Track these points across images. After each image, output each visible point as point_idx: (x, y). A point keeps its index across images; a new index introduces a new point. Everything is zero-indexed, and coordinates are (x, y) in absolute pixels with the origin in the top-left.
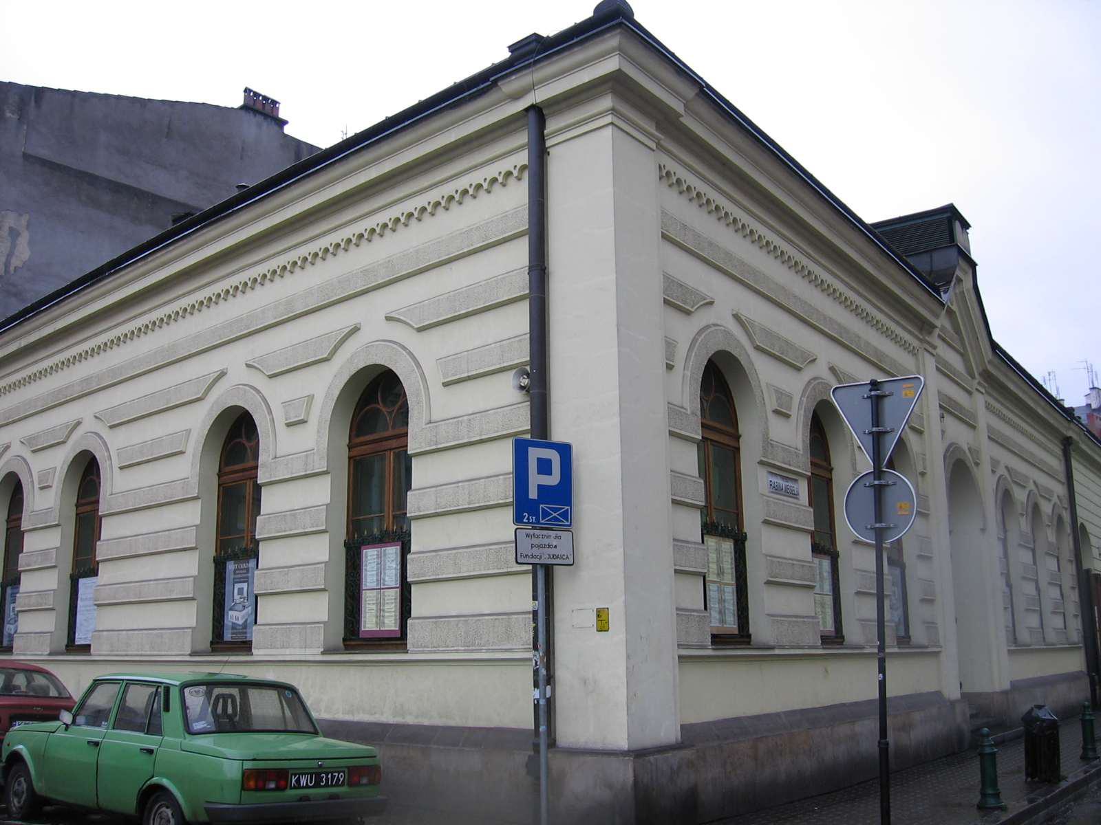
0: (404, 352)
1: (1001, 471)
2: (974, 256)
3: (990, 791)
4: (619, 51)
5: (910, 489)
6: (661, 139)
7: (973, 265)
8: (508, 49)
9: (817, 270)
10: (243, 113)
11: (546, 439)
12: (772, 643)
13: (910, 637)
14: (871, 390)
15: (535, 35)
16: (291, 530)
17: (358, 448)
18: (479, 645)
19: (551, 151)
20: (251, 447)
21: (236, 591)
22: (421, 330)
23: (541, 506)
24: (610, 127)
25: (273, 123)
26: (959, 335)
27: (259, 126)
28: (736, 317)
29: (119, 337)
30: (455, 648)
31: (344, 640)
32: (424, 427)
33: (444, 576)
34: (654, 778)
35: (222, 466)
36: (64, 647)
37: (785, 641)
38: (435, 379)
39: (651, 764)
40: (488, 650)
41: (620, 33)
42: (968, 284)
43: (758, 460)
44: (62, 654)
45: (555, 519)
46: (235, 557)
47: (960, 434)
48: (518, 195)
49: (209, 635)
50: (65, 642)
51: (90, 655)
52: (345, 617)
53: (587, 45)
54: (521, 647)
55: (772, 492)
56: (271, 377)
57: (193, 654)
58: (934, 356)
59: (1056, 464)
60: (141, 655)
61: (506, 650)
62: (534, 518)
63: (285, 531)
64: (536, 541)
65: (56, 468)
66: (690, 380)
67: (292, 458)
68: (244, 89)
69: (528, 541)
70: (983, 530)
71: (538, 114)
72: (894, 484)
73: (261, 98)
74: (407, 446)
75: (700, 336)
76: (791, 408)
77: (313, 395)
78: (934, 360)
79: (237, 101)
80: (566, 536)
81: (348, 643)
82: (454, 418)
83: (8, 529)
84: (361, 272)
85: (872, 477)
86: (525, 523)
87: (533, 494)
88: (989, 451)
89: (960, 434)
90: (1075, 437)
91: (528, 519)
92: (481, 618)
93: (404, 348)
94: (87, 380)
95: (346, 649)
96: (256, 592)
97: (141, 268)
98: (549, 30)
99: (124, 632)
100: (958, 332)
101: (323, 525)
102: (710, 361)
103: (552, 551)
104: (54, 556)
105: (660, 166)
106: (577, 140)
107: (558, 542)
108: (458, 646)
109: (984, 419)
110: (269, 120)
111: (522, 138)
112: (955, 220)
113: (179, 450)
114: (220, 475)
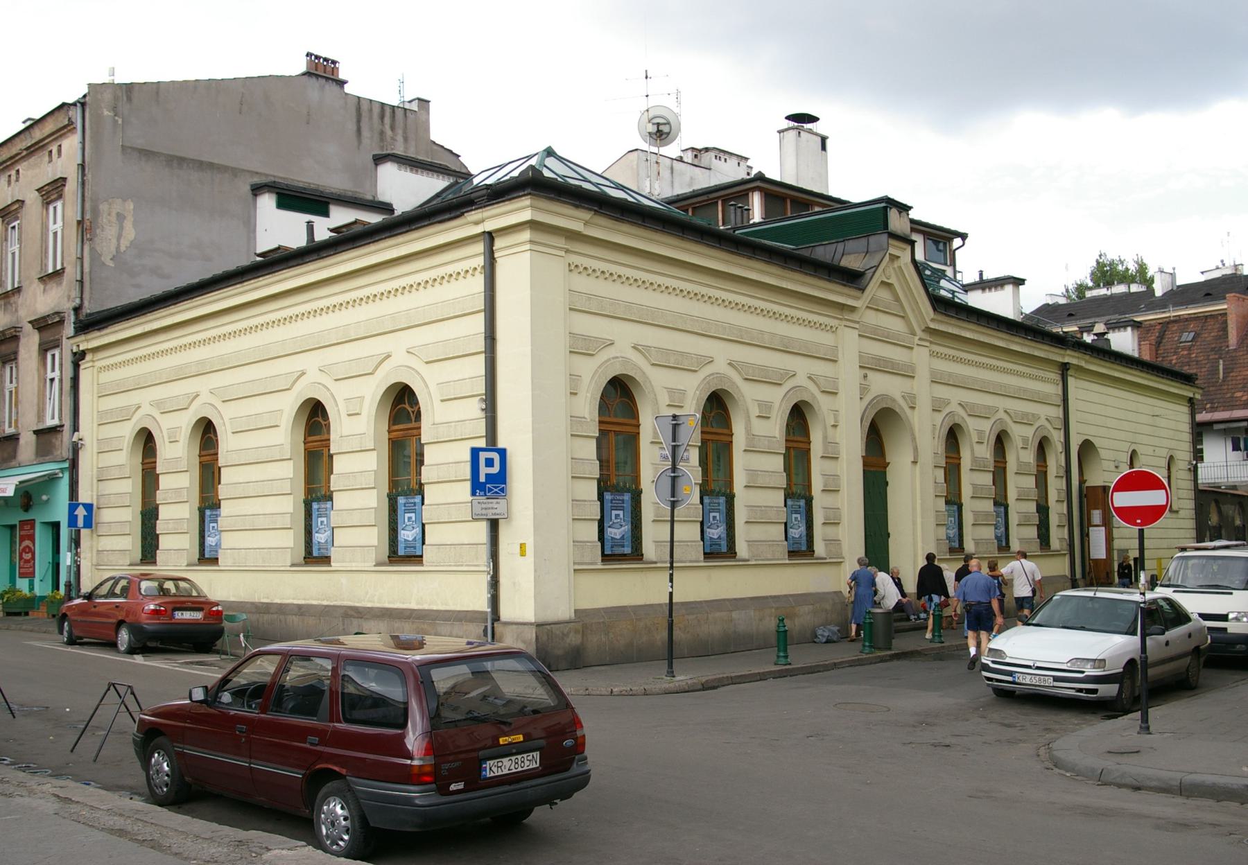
3: (782, 654)
10: (306, 78)
12: (655, 560)
18: (462, 562)
20: (325, 425)
21: (318, 522)
23: (488, 485)
25: (334, 83)
27: (322, 87)
31: (389, 557)
36: (197, 560)
38: (437, 398)
40: (467, 565)
41: (531, 198)
44: (196, 565)
45: (496, 492)
46: (318, 500)
47: (886, 386)
48: (478, 283)
49: (301, 552)
50: (197, 556)
57: (293, 565)
58: (857, 329)
64: (484, 506)
65: (181, 427)
71: (490, 237)
72: (683, 475)
73: (321, 60)
79: (301, 66)
80: (503, 502)
83: (143, 470)
85: (670, 471)
87: (482, 479)
93: (418, 373)
94: (200, 362)
96: (332, 525)
97: (238, 288)
99: (243, 550)
103: (494, 511)
104: (186, 494)
107: (496, 507)
111: (480, 247)
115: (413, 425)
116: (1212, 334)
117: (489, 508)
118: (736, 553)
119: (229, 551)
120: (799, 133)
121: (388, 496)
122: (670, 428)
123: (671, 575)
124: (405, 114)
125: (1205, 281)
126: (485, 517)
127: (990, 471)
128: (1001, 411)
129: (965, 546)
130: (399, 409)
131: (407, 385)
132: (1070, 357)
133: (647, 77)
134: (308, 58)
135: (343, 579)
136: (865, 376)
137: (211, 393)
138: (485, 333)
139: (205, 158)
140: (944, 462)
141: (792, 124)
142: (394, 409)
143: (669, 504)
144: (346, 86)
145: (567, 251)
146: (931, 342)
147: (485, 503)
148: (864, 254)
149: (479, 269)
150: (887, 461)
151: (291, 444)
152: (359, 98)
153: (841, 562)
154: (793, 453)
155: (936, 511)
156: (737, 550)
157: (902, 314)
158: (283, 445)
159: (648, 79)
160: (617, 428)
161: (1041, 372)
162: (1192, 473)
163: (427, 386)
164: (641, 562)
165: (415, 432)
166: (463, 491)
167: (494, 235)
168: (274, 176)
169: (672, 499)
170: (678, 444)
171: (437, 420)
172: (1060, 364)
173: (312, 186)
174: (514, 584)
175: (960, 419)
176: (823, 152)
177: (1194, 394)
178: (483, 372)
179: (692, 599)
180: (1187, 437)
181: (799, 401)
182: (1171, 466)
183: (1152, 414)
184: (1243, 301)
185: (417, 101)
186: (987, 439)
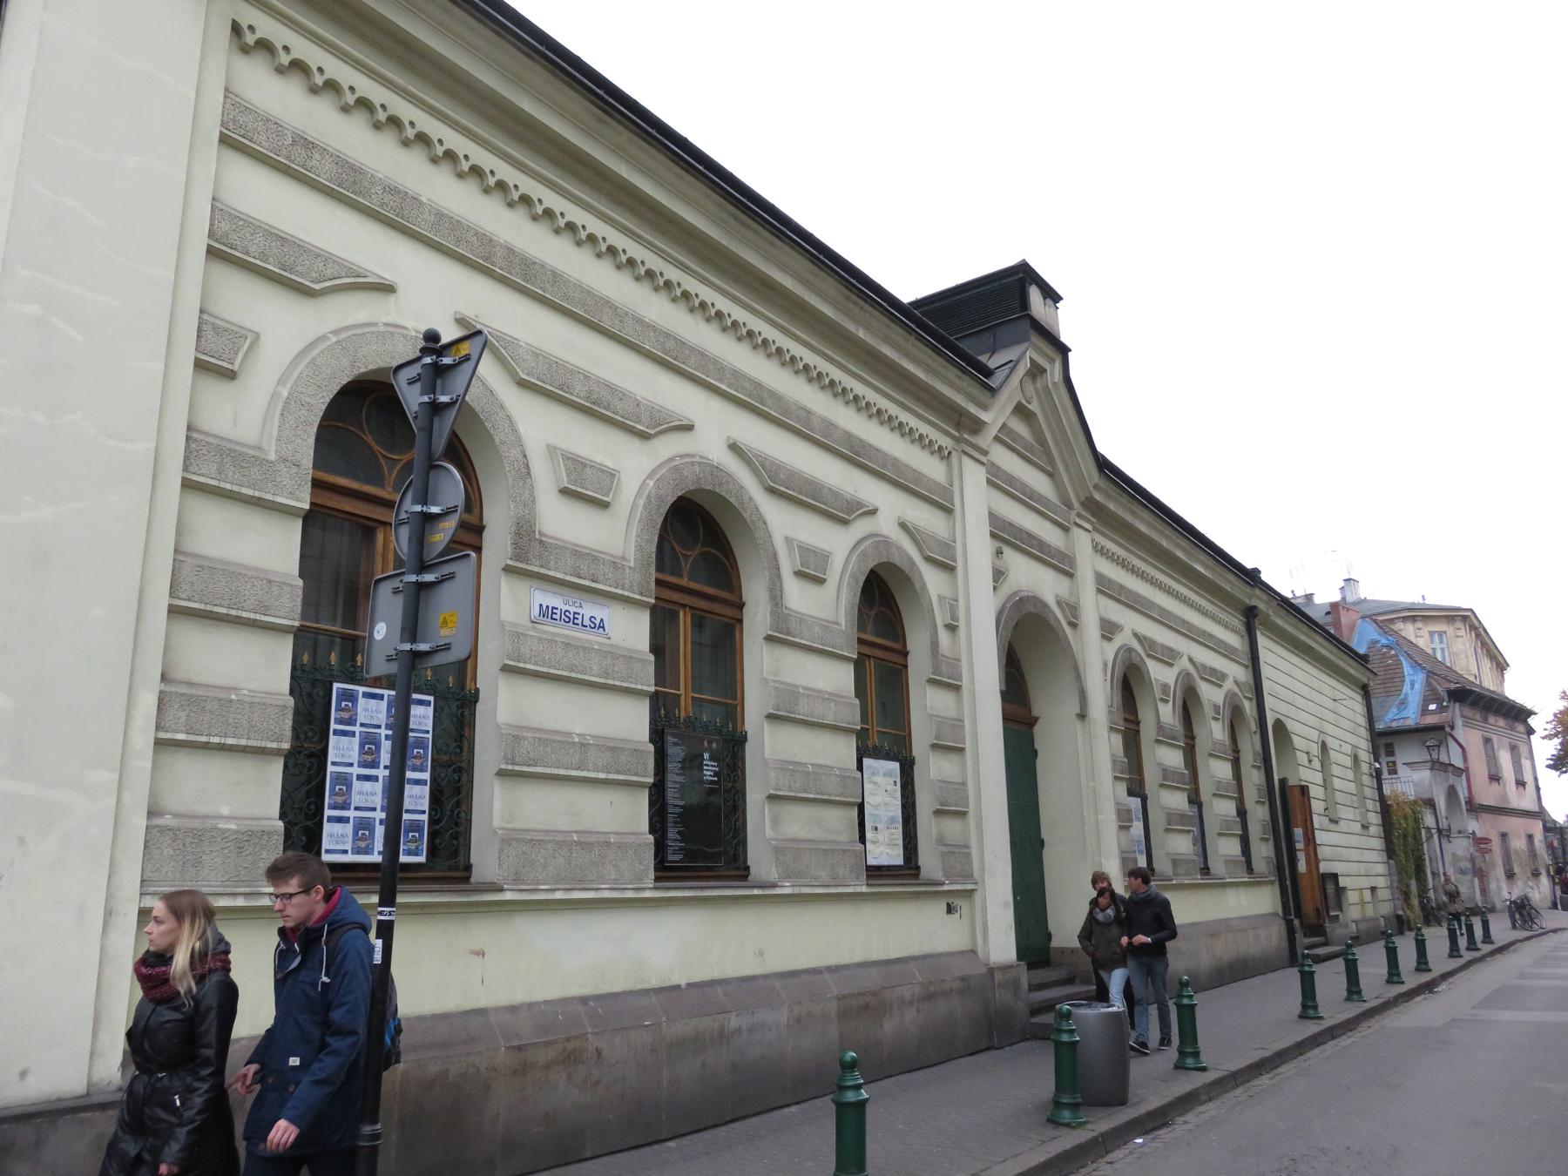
2: (1065, 338)
7: (1064, 350)
9: (706, 294)
13: (1208, 869)
42: (1056, 373)
43: (503, 566)
47: (1030, 577)
58: (983, 464)
59: (1235, 641)
70: (1082, 716)
76: (825, 570)
78: (984, 470)
89: (1030, 577)
90: (1262, 606)
102: (872, 571)
109: (1088, 563)
112: (1031, 284)
118: (747, 868)
127: (286, 511)
128: (1185, 658)
136: (999, 553)
154: (870, 666)
156: (750, 863)
161: (1225, 614)
162: (1375, 780)
164: (464, 886)
175: (1138, 659)
179: (618, 986)
181: (878, 565)
182: (1236, 728)
186: (1172, 696)
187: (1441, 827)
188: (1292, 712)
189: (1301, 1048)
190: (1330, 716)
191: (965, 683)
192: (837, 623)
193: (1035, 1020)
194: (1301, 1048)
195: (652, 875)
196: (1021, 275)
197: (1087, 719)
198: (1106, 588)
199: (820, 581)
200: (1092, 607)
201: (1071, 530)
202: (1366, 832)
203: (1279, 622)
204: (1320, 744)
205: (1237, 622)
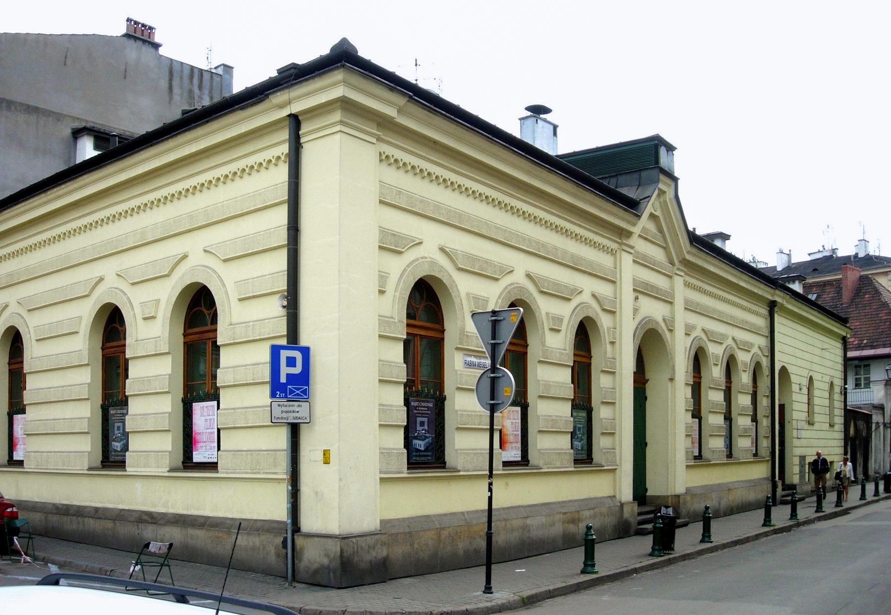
0: (215, 276)
1: (697, 333)
2: (676, 174)
4: (344, 82)
5: (511, 379)
6: (380, 135)
7: (675, 180)
8: (276, 71)
11: (297, 345)
14: (492, 316)
15: (293, 64)
16: (148, 390)
17: (190, 337)
19: (305, 146)
22: (225, 261)
23: (288, 387)
24: (340, 133)
25: (150, 46)
26: (661, 233)
28: (442, 250)
29: (31, 245)
30: (246, 471)
31: (183, 463)
32: (227, 327)
33: (239, 426)
34: (356, 550)
35: (104, 342)
36: (6, 462)
37: (470, 466)
38: (234, 297)
39: (353, 543)
40: (264, 473)
42: (670, 194)
45: (298, 394)
47: (654, 310)
48: (282, 173)
49: (99, 457)
51: (24, 468)
52: (184, 449)
53: (323, 77)
54: (282, 471)
55: (466, 368)
56: (133, 284)
57: (90, 469)
58: (631, 253)
59: (761, 323)
60: (57, 469)
61: (274, 473)
62: (284, 394)
63: (144, 391)
64: (284, 409)
66: (399, 299)
67: (147, 342)
68: (126, 19)
69: (280, 409)
71: (295, 121)
72: (503, 376)
73: (140, 26)
74: (217, 338)
75: (409, 268)
77: (160, 299)
79: (120, 29)
80: (305, 405)
81: (185, 465)
82: (244, 323)
84: (188, 216)
85: (490, 371)
86: (278, 398)
87: (283, 379)
88: (682, 318)
90: (779, 300)
91: (280, 395)
92: (260, 453)
93: (215, 272)
94: (10, 275)
95: (184, 469)
98: (304, 58)
100: (661, 230)
101: (166, 388)
105: (380, 153)
106: (319, 140)
107: (299, 411)
108: (247, 469)
110: (147, 44)
111: (285, 135)
112: (661, 146)
113: (75, 331)
114: (103, 349)
115: (209, 327)
116: (830, 296)
117: (290, 412)
118: (529, 461)
119: (32, 454)
120: (537, 120)
121: (182, 401)
122: (489, 326)
123: (491, 484)
124: (212, 77)
125: (811, 261)
126: (285, 421)
128: (730, 338)
129: (702, 454)
130: (195, 312)
131: (205, 286)
132: (779, 297)
133: (416, 65)
134: (128, 23)
135: (138, 485)
136: (637, 298)
137: (19, 303)
138: (288, 224)
139: (32, 103)
140: (692, 381)
141: (529, 113)
142: (190, 312)
143: (489, 407)
144: (160, 49)
145: (379, 139)
146: (686, 274)
147: (286, 406)
148: (637, 187)
149: (283, 158)
150: (646, 378)
151: (89, 349)
152: (171, 60)
153: (616, 469)
155: (686, 423)
157: (664, 245)
158: (81, 350)
159: (418, 66)
160: (422, 332)
162: (843, 396)
163: (224, 285)
165: (211, 335)
166: (262, 396)
167: (300, 118)
168: (93, 123)
169: (492, 402)
170: (499, 342)
171: (234, 321)
172: (768, 302)
173: (127, 133)
174: (317, 494)
176: (555, 138)
177: (847, 334)
178: (285, 267)
180: (840, 367)
181: (515, 300)
183: (821, 348)
184: (853, 271)
185: (222, 66)
186: (720, 361)
187: (886, 422)
188: (793, 360)
189: (701, 553)
190: (816, 359)
191: (617, 371)
192: (565, 350)
193: (639, 527)
194: (701, 553)
195: (502, 466)
196: (656, 142)
197: (674, 381)
198: (690, 308)
199: (558, 331)
200: (682, 318)
201: (673, 278)
202: (832, 429)
203: (790, 307)
204: (808, 378)
205: (764, 311)
